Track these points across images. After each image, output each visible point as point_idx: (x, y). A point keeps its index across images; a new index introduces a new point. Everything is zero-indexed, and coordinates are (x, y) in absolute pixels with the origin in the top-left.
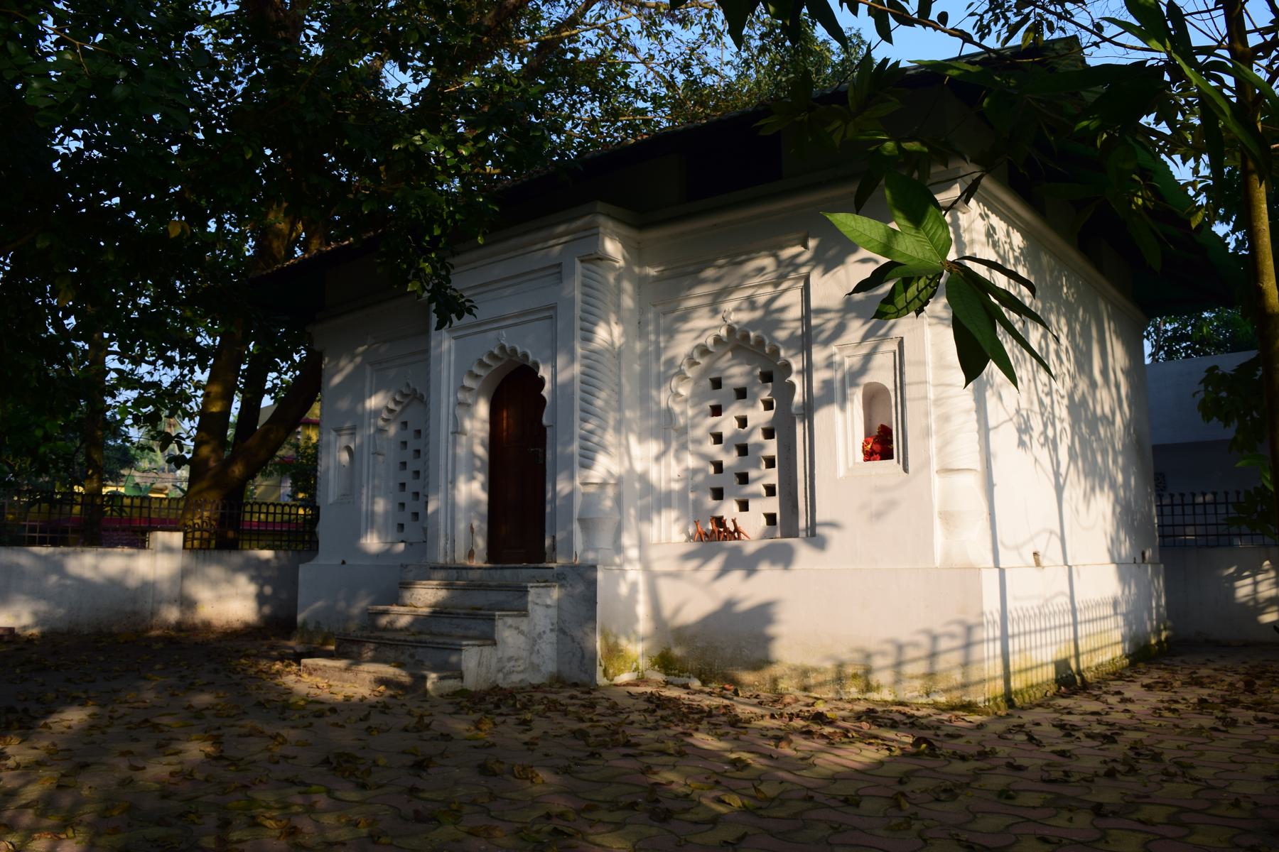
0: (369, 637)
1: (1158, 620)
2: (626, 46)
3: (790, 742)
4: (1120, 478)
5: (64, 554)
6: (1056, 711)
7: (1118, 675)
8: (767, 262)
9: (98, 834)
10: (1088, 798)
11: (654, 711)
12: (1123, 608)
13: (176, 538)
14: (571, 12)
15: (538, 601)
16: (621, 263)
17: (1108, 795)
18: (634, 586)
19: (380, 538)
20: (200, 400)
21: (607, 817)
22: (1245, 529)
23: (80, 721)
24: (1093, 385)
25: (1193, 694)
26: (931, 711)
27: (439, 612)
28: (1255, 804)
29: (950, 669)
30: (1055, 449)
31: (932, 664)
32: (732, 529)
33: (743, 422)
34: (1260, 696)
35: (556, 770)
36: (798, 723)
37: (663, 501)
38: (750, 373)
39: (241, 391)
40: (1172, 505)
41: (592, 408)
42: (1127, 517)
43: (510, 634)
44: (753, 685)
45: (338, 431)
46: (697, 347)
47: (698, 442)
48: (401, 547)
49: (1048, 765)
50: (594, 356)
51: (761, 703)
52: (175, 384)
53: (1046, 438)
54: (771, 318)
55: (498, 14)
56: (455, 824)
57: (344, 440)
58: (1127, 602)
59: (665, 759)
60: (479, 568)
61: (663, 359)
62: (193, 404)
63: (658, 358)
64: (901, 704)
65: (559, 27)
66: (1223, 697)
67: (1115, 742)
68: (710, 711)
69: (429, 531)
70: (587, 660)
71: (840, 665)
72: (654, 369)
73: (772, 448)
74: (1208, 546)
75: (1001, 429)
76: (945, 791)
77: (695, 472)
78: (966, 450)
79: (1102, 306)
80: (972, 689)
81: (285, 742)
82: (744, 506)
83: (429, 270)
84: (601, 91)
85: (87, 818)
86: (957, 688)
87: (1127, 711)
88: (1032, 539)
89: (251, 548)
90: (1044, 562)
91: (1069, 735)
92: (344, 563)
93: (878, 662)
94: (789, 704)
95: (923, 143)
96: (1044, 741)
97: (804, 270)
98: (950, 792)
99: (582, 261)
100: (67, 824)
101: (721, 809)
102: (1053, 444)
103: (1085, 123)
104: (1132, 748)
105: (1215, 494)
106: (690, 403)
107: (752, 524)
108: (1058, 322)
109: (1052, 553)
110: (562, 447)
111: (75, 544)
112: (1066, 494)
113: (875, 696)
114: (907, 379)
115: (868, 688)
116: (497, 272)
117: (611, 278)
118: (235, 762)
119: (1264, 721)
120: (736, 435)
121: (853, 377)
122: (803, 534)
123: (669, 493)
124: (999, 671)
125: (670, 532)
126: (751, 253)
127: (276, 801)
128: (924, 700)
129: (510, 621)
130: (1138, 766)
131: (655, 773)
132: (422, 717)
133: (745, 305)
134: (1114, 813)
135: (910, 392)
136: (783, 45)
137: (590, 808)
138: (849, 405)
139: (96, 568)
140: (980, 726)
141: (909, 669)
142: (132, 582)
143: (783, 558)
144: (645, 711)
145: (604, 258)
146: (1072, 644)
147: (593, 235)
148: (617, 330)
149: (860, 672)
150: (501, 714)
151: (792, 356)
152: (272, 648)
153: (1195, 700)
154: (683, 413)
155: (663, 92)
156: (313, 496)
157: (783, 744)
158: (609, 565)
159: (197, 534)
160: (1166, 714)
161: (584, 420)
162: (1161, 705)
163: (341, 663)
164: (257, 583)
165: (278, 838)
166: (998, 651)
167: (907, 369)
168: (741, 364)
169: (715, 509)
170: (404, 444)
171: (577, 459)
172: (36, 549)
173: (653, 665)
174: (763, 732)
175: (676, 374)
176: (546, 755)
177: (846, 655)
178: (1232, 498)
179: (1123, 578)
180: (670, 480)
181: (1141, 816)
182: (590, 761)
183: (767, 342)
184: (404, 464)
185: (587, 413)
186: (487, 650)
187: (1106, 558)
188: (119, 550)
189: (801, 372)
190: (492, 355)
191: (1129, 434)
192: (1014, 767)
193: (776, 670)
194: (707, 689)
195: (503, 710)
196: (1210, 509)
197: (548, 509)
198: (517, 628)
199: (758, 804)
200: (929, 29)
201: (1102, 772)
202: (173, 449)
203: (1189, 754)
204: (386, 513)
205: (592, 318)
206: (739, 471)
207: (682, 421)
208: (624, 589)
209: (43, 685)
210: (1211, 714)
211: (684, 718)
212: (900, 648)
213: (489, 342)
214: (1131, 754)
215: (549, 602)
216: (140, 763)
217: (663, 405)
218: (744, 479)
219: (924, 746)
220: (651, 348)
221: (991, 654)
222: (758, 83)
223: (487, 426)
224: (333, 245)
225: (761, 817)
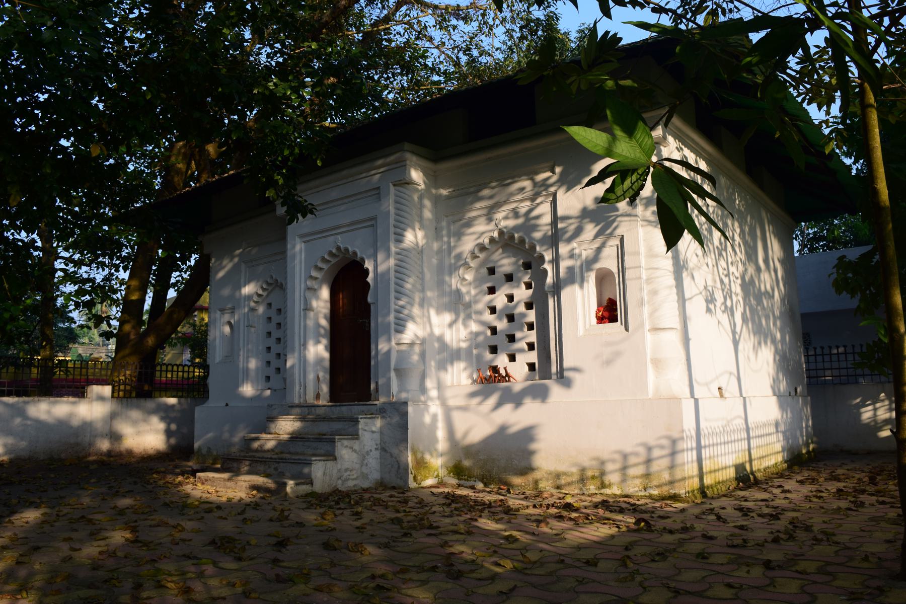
0: (245, 456)
1: (807, 436)
2: (425, 36)
3: (548, 523)
4: (778, 336)
5: (28, 403)
6: (736, 499)
7: (780, 475)
8: (527, 184)
9: (46, 595)
10: (760, 557)
11: (450, 504)
12: (782, 428)
13: (107, 390)
14: (385, 12)
15: (366, 428)
16: (423, 186)
17: (774, 555)
18: (434, 417)
19: (253, 387)
20: (123, 293)
21: (415, 577)
22: (867, 371)
23: (35, 518)
24: (758, 270)
25: (833, 486)
26: (648, 501)
27: (295, 437)
28: (879, 558)
29: (661, 471)
30: (733, 315)
31: (648, 468)
32: (504, 374)
33: (511, 298)
34: (881, 486)
35: (379, 546)
36: (553, 511)
37: (455, 355)
38: (516, 263)
39: (153, 285)
40: (815, 355)
41: (402, 290)
42: (784, 363)
43: (346, 452)
44: (521, 486)
45: (222, 311)
46: (477, 245)
47: (480, 313)
48: (268, 392)
49: (731, 535)
50: (405, 253)
51: (526, 498)
52: (107, 279)
53: (726, 307)
54: (529, 224)
55: (333, 12)
56: (305, 584)
57: (227, 317)
58: (785, 424)
59: (457, 536)
60: (324, 406)
61: (453, 254)
62: (119, 295)
63: (450, 253)
64: (627, 496)
65: (375, 24)
66: (854, 487)
67: (779, 519)
68: (490, 503)
69: (288, 381)
70: (402, 470)
71: (583, 470)
72: (447, 262)
73: (532, 316)
74: (841, 384)
75: (694, 299)
76: (658, 554)
77: (477, 334)
78: (670, 315)
79: (764, 214)
80: (677, 484)
81: (183, 529)
82: (512, 358)
83: (281, 182)
84: (408, 68)
85: (37, 584)
86: (666, 484)
87: (786, 498)
88: (717, 378)
89: (161, 397)
90: (726, 394)
91: (746, 515)
92: (227, 405)
93: (610, 467)
94: (547, 498)
95: (634, 81)
96: (728, 520)
97: (552, 189)
98: (662, 555)
99: (394, 185)
100: (24, 588)
101: (498, 570)
102: (731, 311)
103: (749, 59)
104: (791, 523)
105: (845, 347)
106: (472, 286)
107: (518, 371)
108: (733, 225)
109: (731, 388)
110: (381, 318)
111: (34, 395)
112: (741, 347)
113: (608, 491)
114: (627, 265)
115: (603, 486)
116: (334, 194)
117: (416, 197)
118: (146, 544)
119: (883, 503)
120: (506, 307)
121: (589, 264)
122: (554, 377)
123: (459, 350)
124: (695, 471)
125: (459, 378)
126: (515, 177)
127: (176, 570)
128: (643, 493)
129: (346, 443)
130: (795, 535)
131: (451, 546)
132: (282, 511)
133: (511, 215)
134: (779, 566)
135: (629, 274)
136: (536, 34)
137: (404, 571)
138: (586, 285)
139: (49, 412)
140: (683, 510)
141: (632, 472)
142: (75, 423)
143: (541, 394)
144: (443, 504)
145: (410, 183)
146: (747, 453)
147: (402, 167)
148: (420, 234)
149: (597, 474)
150: (340, 509)
151: (545, 250)
152: (176, 467)
153: (835, 490)
154: (468, 292)
155: (452, 69)
156: (205, 360)
157: (542, 525)
158: (416, 401)
159: (122, 387)
160: (815, 500)
161: (398, 299)
162: (810, 494)
163: (226, 476)
164: (165, 422)
165: (177, 596)
166: (695, 458)
167: (626, 258)
168: (508, 257)
169: (492, 360)
170: (270, 319)
171: (393, 326)
172: (5, 399)
173: (449, 473)
174: (528, 518)
175: (463, 265)
176: (372, 535)
177: (586, 463)
178: (858, 350)
179: (782, 406)
180: (459, 341)
181: (799, 568)
182: (404, 539)
183: (527, 241)
184: (269, 334)
185: (400, 293)
186: (330, 464)
187: (770, 392)
188: (65, 399)
189: (551, 262)
190: (331, 254)
191: (784, 304)
192: (706, 537)
193: (537, 475)
194: (488, 489)
195: (342, 505)
196: (842, 357)
197: (373, 363)
198: (351, 448)
199: (525, 566)
200: (638, 8)
201: (770, 539)
202: (104, 327)
203: (830, 526)
204: (257, 369)
205: (402, 226)
206: (508, 313)
207: (467, 298)
208: (427, 419)
209: (9, 494)
210: (846, 499)
211: (471, 509)
212: (625, 456)
213: (329, 244)
214: (791, 527)
215: (374, 429)
216: (77, 546)
217: (454, 287)
218: (512, 339)
219: (643, 524)
220: (445, 247)
221: (690, 459)
222: (519, 62)
223: (328, 305)
224: (217, 177)
225: (527, 574)
